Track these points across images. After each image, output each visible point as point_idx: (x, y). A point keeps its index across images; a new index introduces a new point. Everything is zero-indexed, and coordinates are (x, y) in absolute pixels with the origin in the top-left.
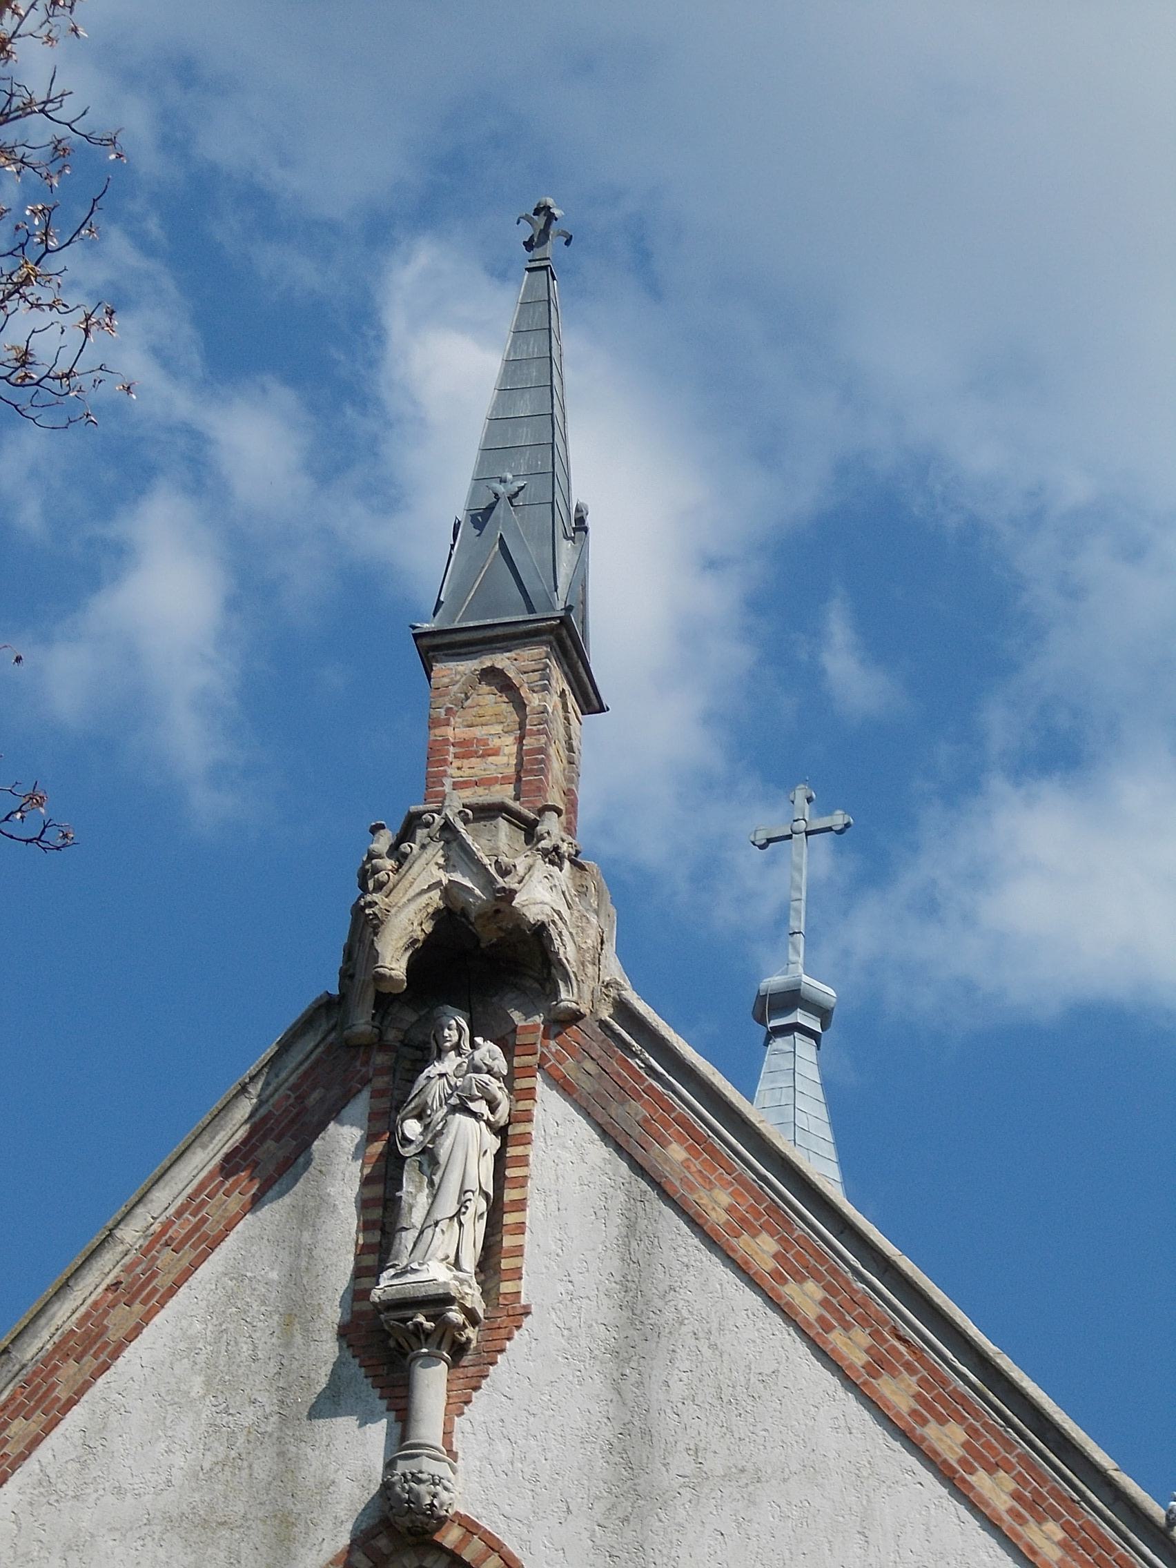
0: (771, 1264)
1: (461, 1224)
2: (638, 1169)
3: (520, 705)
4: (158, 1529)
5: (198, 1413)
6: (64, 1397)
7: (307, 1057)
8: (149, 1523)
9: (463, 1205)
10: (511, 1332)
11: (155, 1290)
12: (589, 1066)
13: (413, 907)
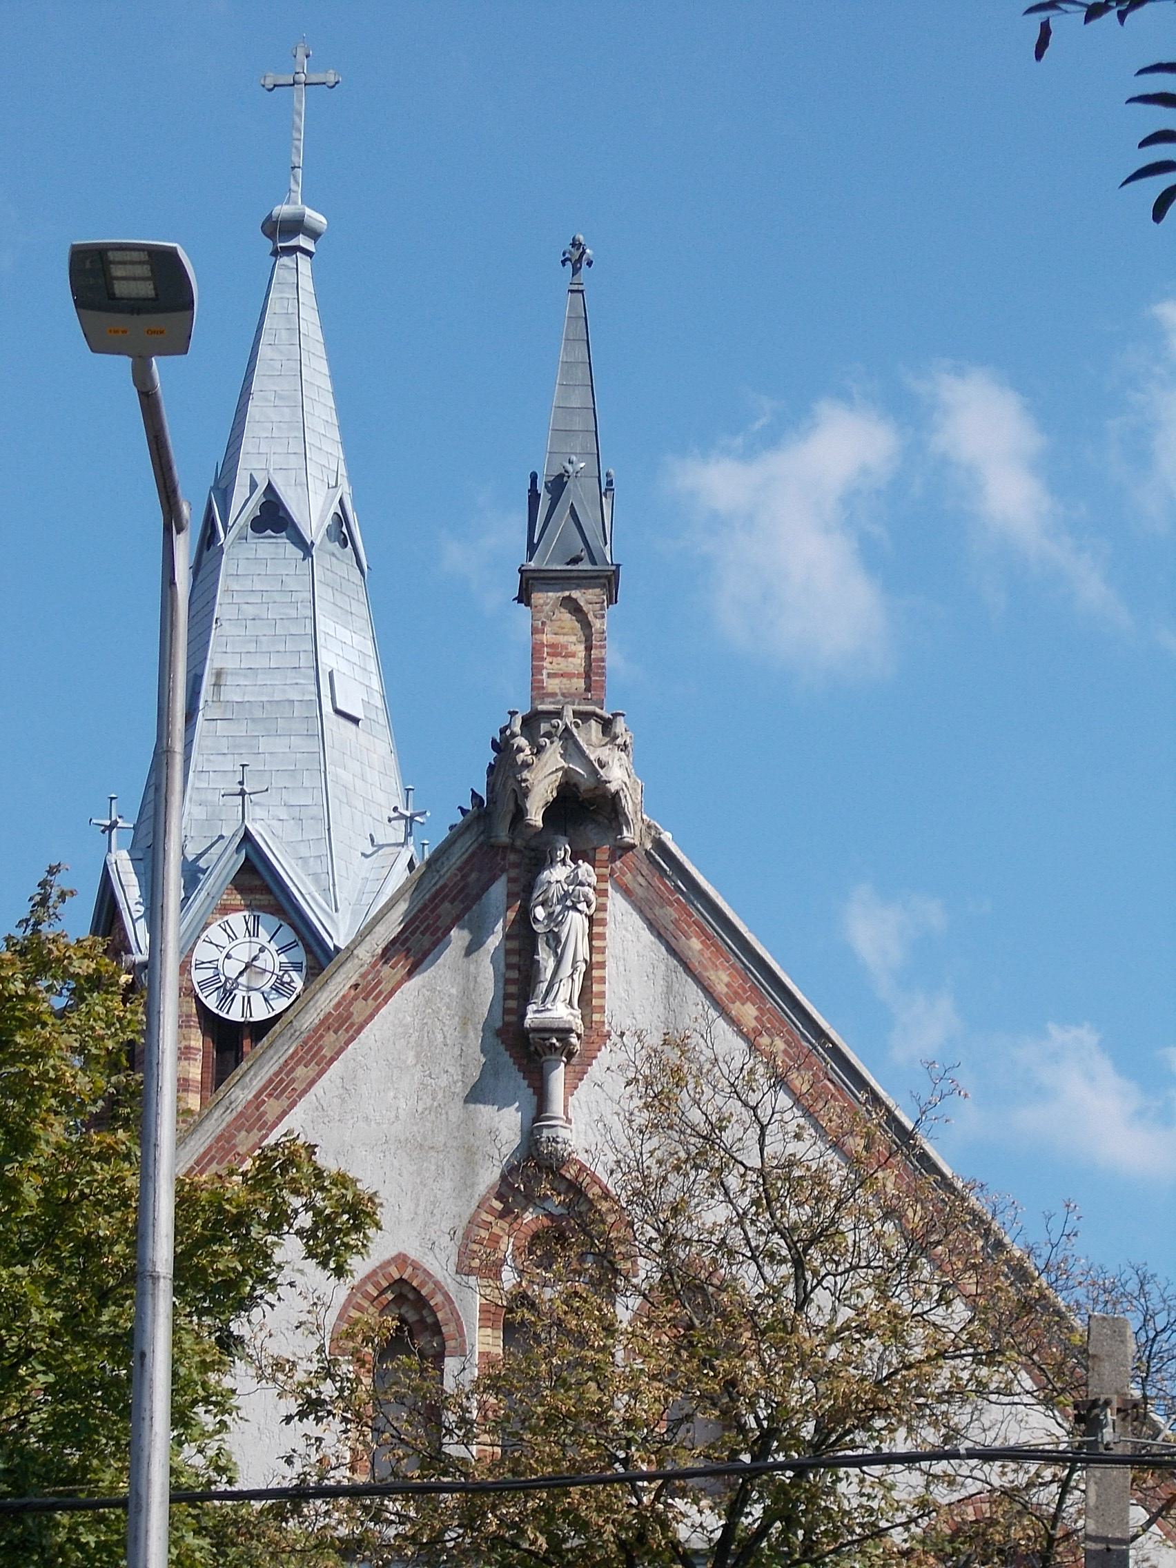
0: (754, 1023)
1: (573, 980)
2: (672, 951)
3: (586, 625)
4: (393, 1148)
5: (413, 1075)
6: (329, 1055)
7: (467, 850)
8: (386, 1142)
9: (575, 969)
10: (600, 1047)
11: (380, 993)
12: (640, 879)
13: (547, 780)
